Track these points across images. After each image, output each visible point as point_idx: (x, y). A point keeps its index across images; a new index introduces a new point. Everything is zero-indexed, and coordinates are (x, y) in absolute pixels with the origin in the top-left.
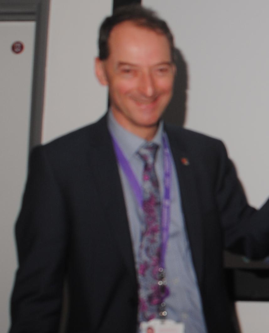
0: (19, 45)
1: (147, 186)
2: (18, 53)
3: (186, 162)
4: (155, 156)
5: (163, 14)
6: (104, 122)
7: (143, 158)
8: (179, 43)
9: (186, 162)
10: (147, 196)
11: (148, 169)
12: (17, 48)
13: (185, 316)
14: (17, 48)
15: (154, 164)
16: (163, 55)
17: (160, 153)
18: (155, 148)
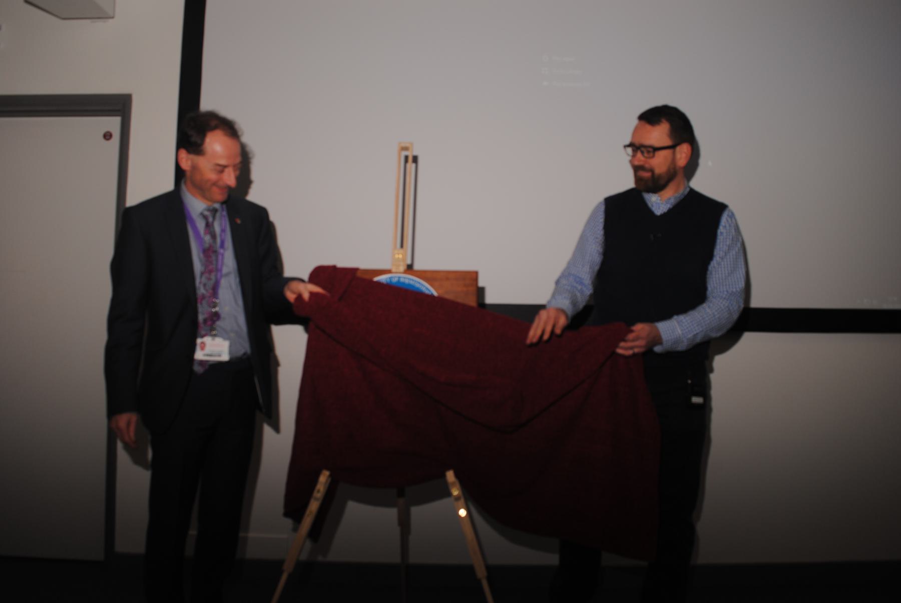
0: (109, 134)
1: (207, 238)
2: (108, 139)
3: (239, 221)
4: (214, 217)
8: (245, 139)
9: (239, 221)
10: (207, 246)
11: (208, 226)
12: (108, 136)
13: (232, 335)
14: (108, 136)
17: (218, 215)
18: (214, 211)
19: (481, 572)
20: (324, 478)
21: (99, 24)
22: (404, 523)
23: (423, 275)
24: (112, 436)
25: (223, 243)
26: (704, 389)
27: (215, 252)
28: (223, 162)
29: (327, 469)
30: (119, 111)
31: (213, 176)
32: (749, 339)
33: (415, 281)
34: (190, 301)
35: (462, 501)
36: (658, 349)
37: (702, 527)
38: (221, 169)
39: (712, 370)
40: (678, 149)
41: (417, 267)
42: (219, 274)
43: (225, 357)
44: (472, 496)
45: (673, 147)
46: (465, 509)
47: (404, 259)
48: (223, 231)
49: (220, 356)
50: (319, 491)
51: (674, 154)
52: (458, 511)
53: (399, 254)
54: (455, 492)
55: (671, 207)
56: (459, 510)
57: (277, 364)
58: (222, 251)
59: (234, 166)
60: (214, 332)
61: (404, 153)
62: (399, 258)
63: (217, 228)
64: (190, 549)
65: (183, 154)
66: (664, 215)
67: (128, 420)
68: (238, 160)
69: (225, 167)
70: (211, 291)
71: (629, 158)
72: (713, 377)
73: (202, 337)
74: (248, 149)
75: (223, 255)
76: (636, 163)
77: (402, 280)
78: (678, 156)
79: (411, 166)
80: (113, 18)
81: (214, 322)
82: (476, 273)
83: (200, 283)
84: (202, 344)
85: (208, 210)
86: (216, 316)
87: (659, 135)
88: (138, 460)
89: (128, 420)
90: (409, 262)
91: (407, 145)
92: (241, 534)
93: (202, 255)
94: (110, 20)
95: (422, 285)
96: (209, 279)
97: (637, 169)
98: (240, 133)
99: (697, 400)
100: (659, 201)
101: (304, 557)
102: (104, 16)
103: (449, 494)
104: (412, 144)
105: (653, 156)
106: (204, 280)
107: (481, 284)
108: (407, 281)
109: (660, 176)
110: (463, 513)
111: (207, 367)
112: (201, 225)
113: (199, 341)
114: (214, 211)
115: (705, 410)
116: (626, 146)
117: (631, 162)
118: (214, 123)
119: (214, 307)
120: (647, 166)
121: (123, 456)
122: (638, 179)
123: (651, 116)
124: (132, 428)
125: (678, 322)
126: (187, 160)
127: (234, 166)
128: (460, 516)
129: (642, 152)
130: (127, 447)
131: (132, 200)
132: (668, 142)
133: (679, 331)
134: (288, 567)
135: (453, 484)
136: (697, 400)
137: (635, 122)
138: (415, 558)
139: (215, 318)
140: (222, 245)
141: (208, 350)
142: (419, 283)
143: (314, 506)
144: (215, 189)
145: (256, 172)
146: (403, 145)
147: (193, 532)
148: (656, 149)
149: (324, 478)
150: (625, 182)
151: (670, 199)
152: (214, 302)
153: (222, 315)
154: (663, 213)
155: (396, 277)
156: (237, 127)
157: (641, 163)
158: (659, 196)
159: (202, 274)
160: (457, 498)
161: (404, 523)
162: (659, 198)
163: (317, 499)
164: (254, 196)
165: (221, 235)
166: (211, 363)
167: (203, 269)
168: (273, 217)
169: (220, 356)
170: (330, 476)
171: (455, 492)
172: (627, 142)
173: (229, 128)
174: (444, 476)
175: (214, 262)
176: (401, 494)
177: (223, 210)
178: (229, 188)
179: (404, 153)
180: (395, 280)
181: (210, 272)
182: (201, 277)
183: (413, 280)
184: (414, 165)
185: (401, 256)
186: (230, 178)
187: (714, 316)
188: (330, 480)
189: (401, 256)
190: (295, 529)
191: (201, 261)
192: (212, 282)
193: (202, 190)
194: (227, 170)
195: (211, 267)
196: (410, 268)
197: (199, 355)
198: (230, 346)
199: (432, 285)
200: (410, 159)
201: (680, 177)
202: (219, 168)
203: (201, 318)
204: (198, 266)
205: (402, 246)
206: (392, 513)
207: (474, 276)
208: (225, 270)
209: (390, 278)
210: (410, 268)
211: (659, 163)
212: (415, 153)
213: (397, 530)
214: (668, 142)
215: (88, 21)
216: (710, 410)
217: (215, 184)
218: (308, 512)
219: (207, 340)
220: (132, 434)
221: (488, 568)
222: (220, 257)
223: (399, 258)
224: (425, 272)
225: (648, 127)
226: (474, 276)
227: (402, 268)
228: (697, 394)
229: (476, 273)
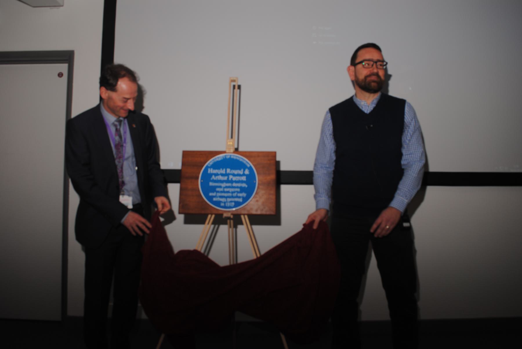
0: (61, 74)
1: (117, 138)
2: (60, 77)
3: (134, 126)
4: (120, 125)
5: (378, 44)
6: (98, 107)
7: (115, 126)
8: (140, 82)
9: (134, 126)
10: (117, 142)
11: (117, 131)
12: (60, 75)
13: (131, 193)
14: (60, 75)
15: (120, 129)
16: (134, 87)
17: (122, 123)
18: (120, 122)
21: (55, 10)
23: (244, 154)
25: (125, 139)
28: (127, 96)
31: (120, 104)
33: (240, 158)
37: (420, 304)
38: (126, 100)
41: (240, 149)
47: (233, 145)
53: (230, 142)
55: (375, 106)
59: (134, 98)
62: (230, 144)
65: (103, 89)
66: (372, 112)
68: (136, 95)
69: (128, 99)
74: (143, 89)
77: (232, 157)
79: (237, 91)
80: (62, 6)
82: (275, 153)
90: (236, 147)
91: (235, 79)
94: (61, 8)
95: (244, 160)
98: (137, 79)
100: (366, 104)
104: (237, 78)
107: (278, 159)
108: (235, 158)
118: (123, 73)
126: (106, 94)
127: (134, 98)
142: (242, 159)
144: (122, 111)
145: (147, 103)
146: (232, 79)
147: (111, 304)
155: (229, 155)
156: (136, 75)
164: (145, 112)
173: (131, 75)
178: (130, 111)
180: (228, 157)
183: (238, 157)
184: (238, 91)
185: (231, 143)
186: (130, 105)
189: (231, 143)
193: (113, 111)
194: (129, 101)
196: (236, 150)
199: (249, 160)
200: (236, 87)
202: (125, 100)
205: (232, 137)
207: (274, 154)
208: (126, 156)
209: (225, 156)
210: (236, 150)
212: (239, 84)
215: (48, 8)
217: (122, 108)
223: (230, 144)
224: (245, 152)
226: (274, 154)
227: (232, 150)
229: (275, 153)
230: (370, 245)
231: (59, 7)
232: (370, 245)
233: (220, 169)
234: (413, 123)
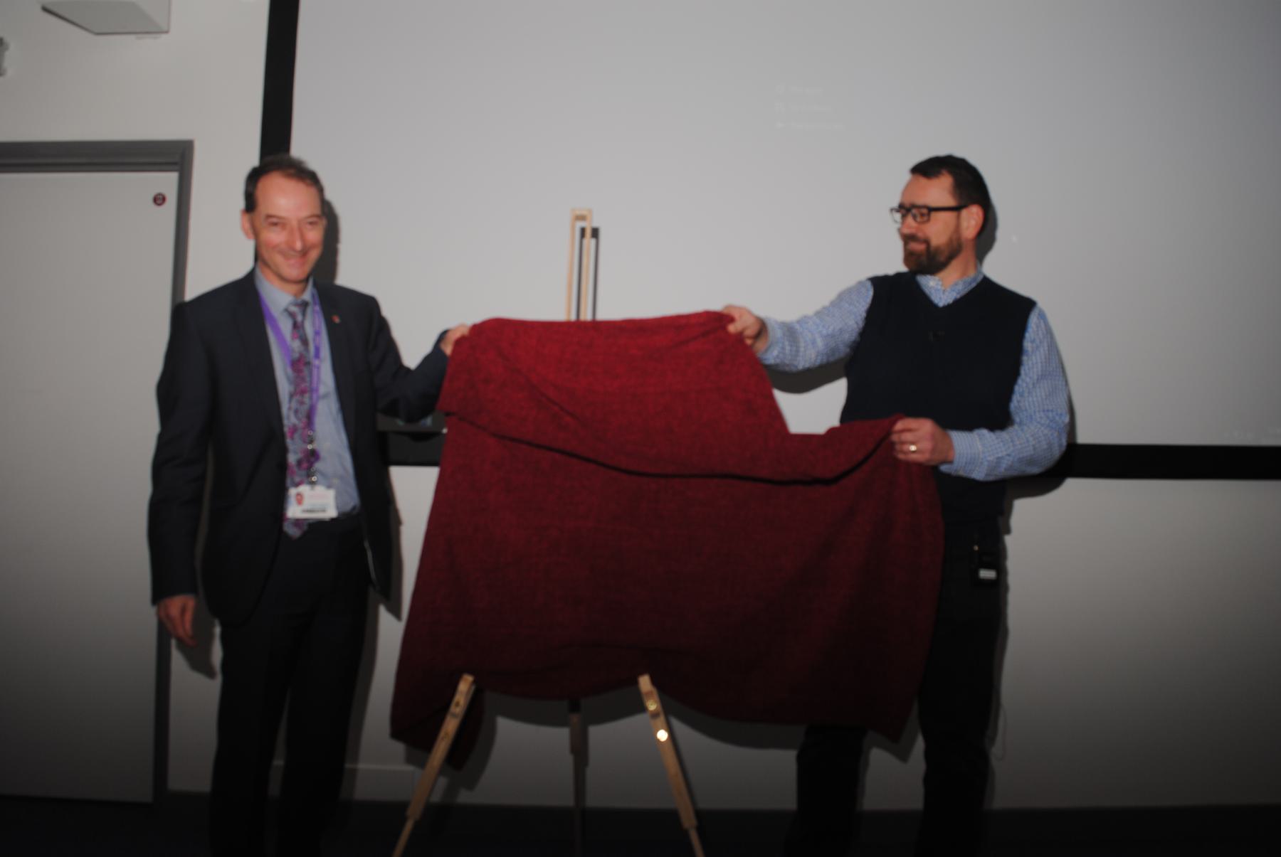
0: (161, 197)
1: (296, 345)
2: (160, 205)
3: (337, 320)
4: (304, 314)
6: (250, 277)
7: (292, 315)
9: (337, 320)
10: (296, 355)
11: (297, 326)
12: (159, 200)
13: (336, 481)
14: (159, 200)
15: (303, 322)
17: (309, 310)
19: (689, 821)
20: (465, 686)
21: (148, 41)
22: (580, 749)
24: (164, 633)
25: (317, 350)
26: (996, 558)
27: (308, 364)
29: (470, 672)
30: (175, 164)
32: (1073, 487)
34: (274, 438)
35: (662, 719)
36: (944, 468)
39: (1008, 531)
40: (964, 213)
42: (315, 396)
43: (331, 513)
44: (669, 712)
45: (957, 209)
46: (666, 730)
48: (317, 333)
49: (324, 511)
50: (457, 704)
51: (958, 218)
52: (656, 733)
54: (652, 706)
56: (657, 731)
57: (398, 522)
58: (317, 362)
60: (314, 479)
61: (580, 224)
63: (309, 330)
64: (275, 788)
66: (948, 308)
67: (182, 606)
70: (304, 420)
71: (898, 226)
72: (1008, 540)
73: (297, 485)
75: (318, 368)
76: (906, 231)
78: (964, 224)
79: (589, 242)
80: (167, 32)
81: (311, 465)
83: (289, 409)
84: (299, 497)
85: (296, 305)
86: (313, 456)
87: (939, 191)
88: (200, 663)
89: (182, 606)
91: (584, 213)
92: (348, 766)
93: (290, 371)
94: (164, 36)
96: (302, 403)
97: (908, 239)
99: (987, 574)
100: (939, 287)
101: (436, 798)
102: (152, 29)
103: (642, 709)
104: (590, 211)
105: (928, 220)
106: (294, 405)
109: (938, 249)
110: (662, 735)
111: (305, 528)
112: (286, 326)
113: (293, 492)
114: (304, 305)
115: (998, 588)
116: (892, 210)
117: (899, 230)
119: (311, 442)
120: (920, 235)
121: (178, 660)
122: (909, 257)
123: (927, 169)
124: (189, 616)
125: (979, 435)
128: (658, 740)
129: (914, 217)
130: (183, 646)
131: (191, 293)
132: (949, 201)
133: (980, 447)
134: (414, 813)
135: (650, 694)
136: (987, 574)
137: (907, 176)
138: (594, 800)
139: (312, 459)
140: (317, 355)
141: (307, 503)
143: (451, 726)
146: (578, 213)
147: (279, 762)
148: (932, 210)
149: (465, 686)
150: (894, 264)
151: (956, 284)
152: (309, 436)
153: (323, 454)
154: (946, 304)
157: (913, 231)
158: (939, 280)
159: (292, 396)
160: (655, 715)
161: (580, 749)
162: (940, 283)
163: (454, 716)
164: (349, 276)
165: (314, 340)
166: (311, 521)
167: (292, 389)
168: (386, 311)
169: (324, 511)
170: (475, 682)
171: (652, 706)
172: (895, 204)
174: (635, 683)
175: (308, 379)
176: (575, 707)
177: (315, 304)
179: (580, 224)
181: (303, 392)
182: (290, 401)
184: (593, 241)
187: (1028, 441)
188: (473, 688)
190: (421, 764)
191: (288, 378)
192: (305, 408)
195: (303, 386)
197: (294, 511)
198: (337, 498)
200: (588, 233)
201: (967, 254)
203: (292, 458)
204: (284, 386)
206: (560, 736)
208: (322, 390)
211: (938, 231)
212: (595, 225)
213: (569, 759)
214: (949, 201)
215: (132, 37)
216: (1006, 588)
218: (442, 734)
219: (304, 489)
220: (188, 625)
221: (699, 814)
222: (315, 372)
225: (923, 181)
228: (988, 566)
230: (173, 642)
231: (158, 35)
232: (173, 642)
233: (740, 337)
234: (1043, 350)
